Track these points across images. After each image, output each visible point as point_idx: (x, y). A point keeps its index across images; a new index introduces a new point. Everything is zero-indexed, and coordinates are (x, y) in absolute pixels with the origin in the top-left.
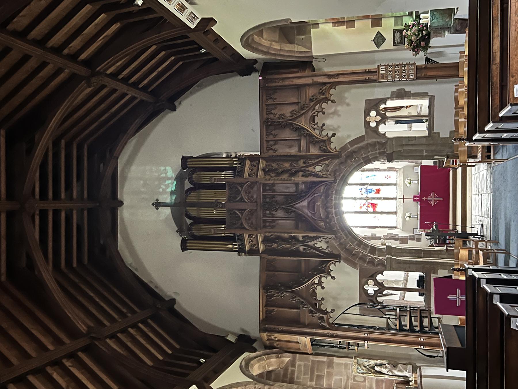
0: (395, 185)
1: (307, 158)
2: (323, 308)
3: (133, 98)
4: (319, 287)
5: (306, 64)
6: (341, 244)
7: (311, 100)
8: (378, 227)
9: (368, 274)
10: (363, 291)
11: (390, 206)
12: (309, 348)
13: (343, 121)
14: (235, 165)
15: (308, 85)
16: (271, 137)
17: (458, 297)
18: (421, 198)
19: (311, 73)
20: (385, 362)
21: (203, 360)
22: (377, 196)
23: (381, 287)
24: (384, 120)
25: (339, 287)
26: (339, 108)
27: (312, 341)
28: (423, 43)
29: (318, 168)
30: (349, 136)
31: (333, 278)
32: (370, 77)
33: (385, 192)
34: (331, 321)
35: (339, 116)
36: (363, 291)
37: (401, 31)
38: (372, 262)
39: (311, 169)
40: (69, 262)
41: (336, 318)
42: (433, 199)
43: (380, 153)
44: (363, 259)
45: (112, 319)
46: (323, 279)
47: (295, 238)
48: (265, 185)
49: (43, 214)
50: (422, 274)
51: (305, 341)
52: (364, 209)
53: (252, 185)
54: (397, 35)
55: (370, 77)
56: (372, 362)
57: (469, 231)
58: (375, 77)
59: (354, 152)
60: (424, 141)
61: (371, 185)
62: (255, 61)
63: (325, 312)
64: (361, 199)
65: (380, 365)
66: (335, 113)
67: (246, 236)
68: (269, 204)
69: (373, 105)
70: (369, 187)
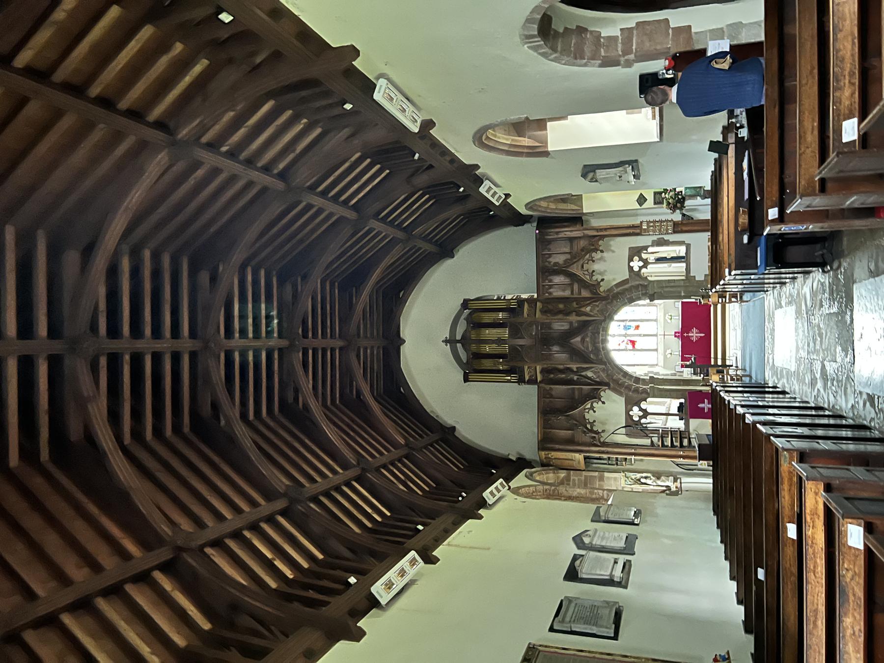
0: (656, 320)
1: (577, 300)
2: (595, 429)
3: (250, 184)
4: (591, 411)
5: (577, 220)
6: (608, 375)
7: (582, 250)
8: (634, 365)
9: (631, 403)
10: (629, 417)
11: (650, 343)
12: (582, 465)
13: (611, 266)
14: (515, 308)
15: (580, 238)
16: (547, 283)
17: (706, 406)
18: (683, 335)
19: (581, 228)
20: (649, 475)
21: (420, 527)
22: (637, 332)
23: (646, 414)
24: (646, 263)
25: (608, 412)
26: (605, 254)
27: (585, 458)
28: (679, 205)
29: (588, 309)
30: (614, 279)
31: (603, 403)
32: (635, 230)
33: (645, 328)
34: (602, 440)
35: (605, 261)
36: (629, 417)
37: (661, 193)
38: (636, 390)
39: (583, 309)
40: (258, 412)
41: (604, 437)
42: (695, 335)
43: (643, 294)
44: (628, 388)
45: (237, 510)
46: (595, 405)
47: (570, 370)
48: (543, 324)
49: (114, 360)
50: (683, 401)
51: (579, 457)
52: (623, 346)
53: (531, 324)
54: (658, 196)
55: (635, 230)
56: (638, 476)
57: (728, 363)
58: (638, 231)
59: (618, 293)
60: (682, 283)
61: (630, 321)
62: (531, 216)
63: (597, 433)
64: (620, 335)
65: (646, 478)
66: (601, 259)
67: (526, 368)
68: (546, 340)
69: (635, 252)
70: (628, 324)
